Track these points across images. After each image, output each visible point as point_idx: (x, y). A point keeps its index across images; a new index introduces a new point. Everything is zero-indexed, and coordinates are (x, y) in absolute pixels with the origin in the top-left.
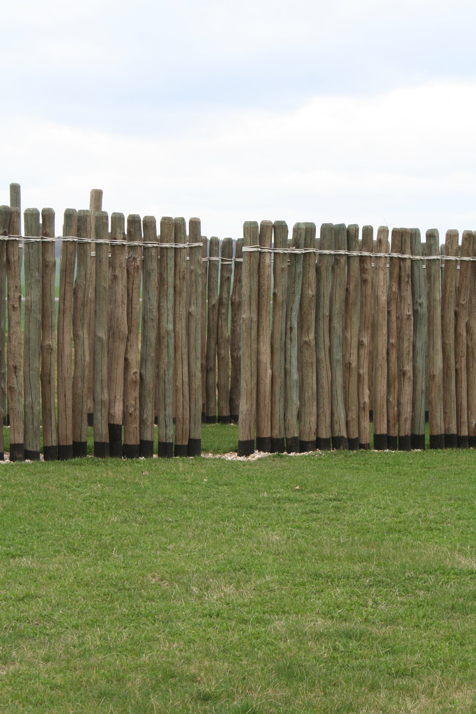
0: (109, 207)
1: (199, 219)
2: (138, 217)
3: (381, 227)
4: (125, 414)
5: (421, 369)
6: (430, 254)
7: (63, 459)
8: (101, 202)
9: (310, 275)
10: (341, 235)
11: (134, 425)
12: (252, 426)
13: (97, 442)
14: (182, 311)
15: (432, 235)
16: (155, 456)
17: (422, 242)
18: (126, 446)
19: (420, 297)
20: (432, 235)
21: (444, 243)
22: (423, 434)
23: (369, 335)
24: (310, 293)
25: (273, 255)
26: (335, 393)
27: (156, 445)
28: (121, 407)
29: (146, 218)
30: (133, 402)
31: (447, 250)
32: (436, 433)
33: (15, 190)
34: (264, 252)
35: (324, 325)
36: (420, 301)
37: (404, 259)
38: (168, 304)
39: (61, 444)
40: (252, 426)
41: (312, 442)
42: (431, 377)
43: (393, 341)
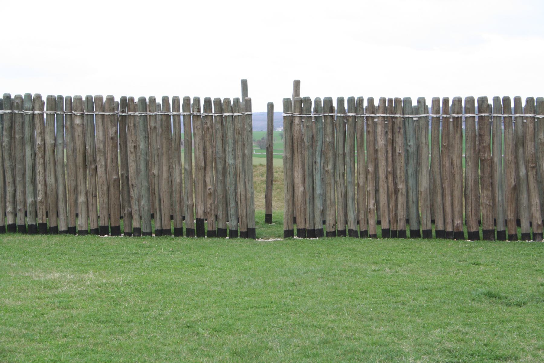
0: (312, 91)
1: (9, 94)
2: (353, 98)
3: (433, 98)
4: (205, 213)
5: (411, 188)
6: (418, 114)
7: (500, 240)
8: (299, 87)
9: (328, 129)
10: (356, 104)
11: (212, 219)
12: (289, 222)
13: (439, 231)
14: (239, 153)
15: (371, 100)
16: (227, 238)
17: (413, 105)
18: (50, 228)
19: (409, 141)
20: (421, 101)
21: (367, 105)
22: (55, 225)
23: (373, 166)
24: (328, 140)
25: (502, 118)
26: (348, 202)
27: (184, 230)
28: (203, 208)
29: (404, 98)
30: (209, 206)
31: (467, 110)
32: (299, 227)
33: (297, 84)
34: (294, 117)
35: (340, 161)
36: (409, 144)
37: (396, 117)
38: (229, 149)
39: (164, 228)
40: (289, 222)
41: (331, 232)
42: (418, 193)
43: (389, 169)
